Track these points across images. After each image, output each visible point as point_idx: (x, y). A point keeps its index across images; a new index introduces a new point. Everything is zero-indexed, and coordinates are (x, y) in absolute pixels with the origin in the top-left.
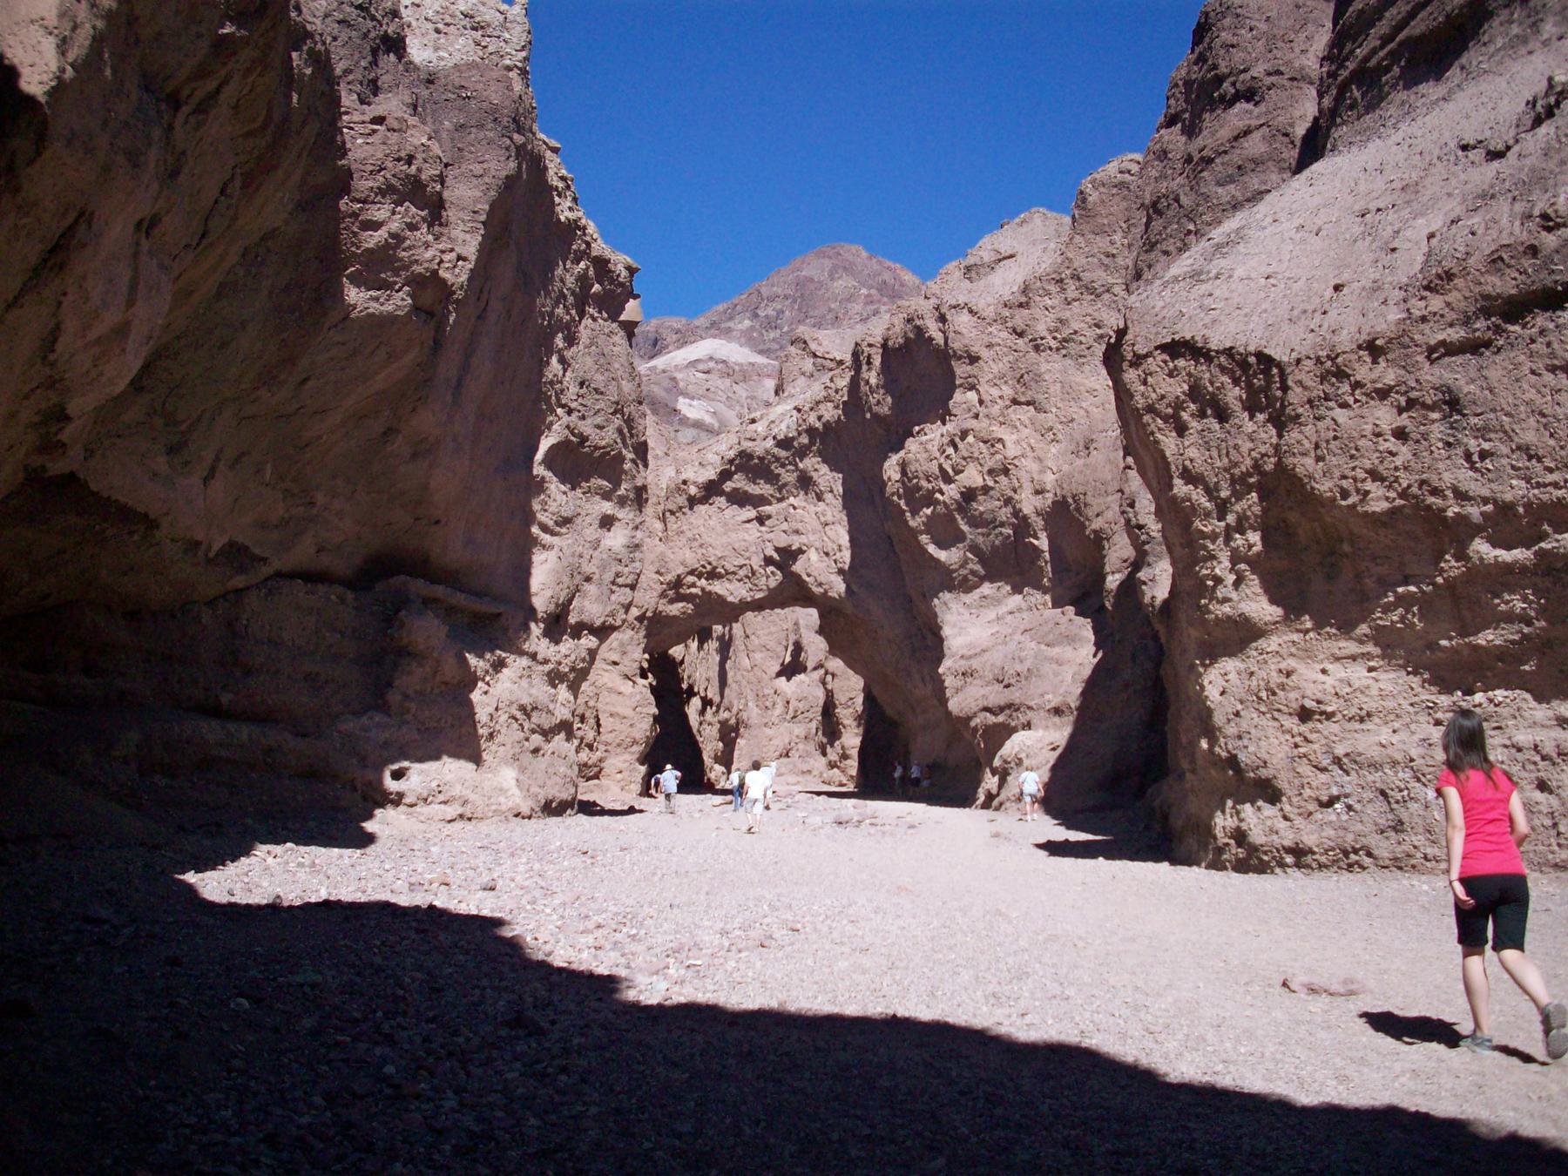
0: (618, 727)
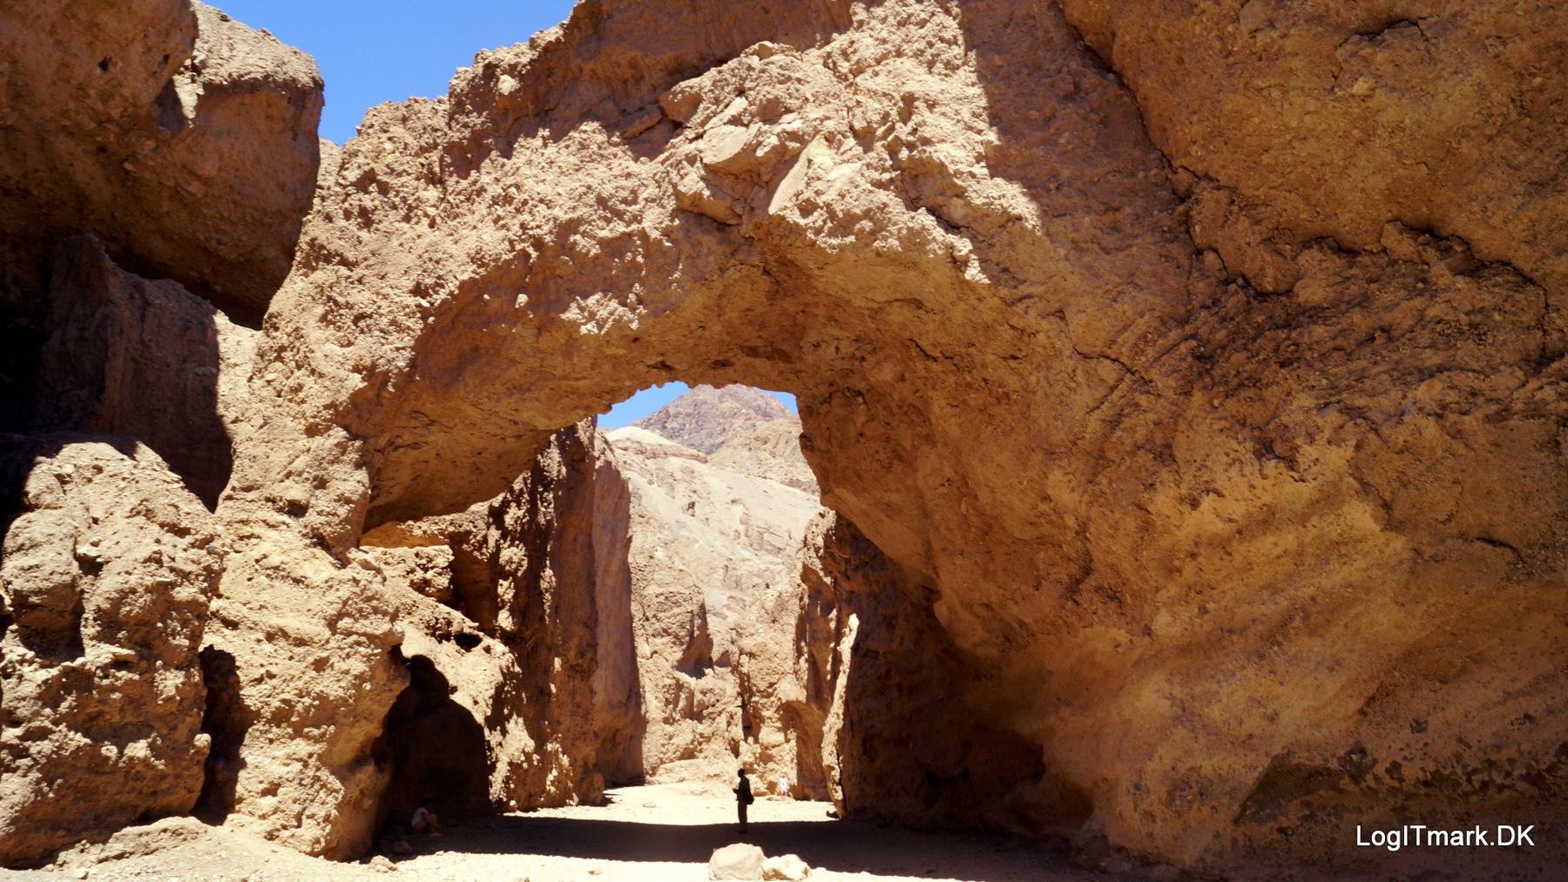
0: (281, 666)
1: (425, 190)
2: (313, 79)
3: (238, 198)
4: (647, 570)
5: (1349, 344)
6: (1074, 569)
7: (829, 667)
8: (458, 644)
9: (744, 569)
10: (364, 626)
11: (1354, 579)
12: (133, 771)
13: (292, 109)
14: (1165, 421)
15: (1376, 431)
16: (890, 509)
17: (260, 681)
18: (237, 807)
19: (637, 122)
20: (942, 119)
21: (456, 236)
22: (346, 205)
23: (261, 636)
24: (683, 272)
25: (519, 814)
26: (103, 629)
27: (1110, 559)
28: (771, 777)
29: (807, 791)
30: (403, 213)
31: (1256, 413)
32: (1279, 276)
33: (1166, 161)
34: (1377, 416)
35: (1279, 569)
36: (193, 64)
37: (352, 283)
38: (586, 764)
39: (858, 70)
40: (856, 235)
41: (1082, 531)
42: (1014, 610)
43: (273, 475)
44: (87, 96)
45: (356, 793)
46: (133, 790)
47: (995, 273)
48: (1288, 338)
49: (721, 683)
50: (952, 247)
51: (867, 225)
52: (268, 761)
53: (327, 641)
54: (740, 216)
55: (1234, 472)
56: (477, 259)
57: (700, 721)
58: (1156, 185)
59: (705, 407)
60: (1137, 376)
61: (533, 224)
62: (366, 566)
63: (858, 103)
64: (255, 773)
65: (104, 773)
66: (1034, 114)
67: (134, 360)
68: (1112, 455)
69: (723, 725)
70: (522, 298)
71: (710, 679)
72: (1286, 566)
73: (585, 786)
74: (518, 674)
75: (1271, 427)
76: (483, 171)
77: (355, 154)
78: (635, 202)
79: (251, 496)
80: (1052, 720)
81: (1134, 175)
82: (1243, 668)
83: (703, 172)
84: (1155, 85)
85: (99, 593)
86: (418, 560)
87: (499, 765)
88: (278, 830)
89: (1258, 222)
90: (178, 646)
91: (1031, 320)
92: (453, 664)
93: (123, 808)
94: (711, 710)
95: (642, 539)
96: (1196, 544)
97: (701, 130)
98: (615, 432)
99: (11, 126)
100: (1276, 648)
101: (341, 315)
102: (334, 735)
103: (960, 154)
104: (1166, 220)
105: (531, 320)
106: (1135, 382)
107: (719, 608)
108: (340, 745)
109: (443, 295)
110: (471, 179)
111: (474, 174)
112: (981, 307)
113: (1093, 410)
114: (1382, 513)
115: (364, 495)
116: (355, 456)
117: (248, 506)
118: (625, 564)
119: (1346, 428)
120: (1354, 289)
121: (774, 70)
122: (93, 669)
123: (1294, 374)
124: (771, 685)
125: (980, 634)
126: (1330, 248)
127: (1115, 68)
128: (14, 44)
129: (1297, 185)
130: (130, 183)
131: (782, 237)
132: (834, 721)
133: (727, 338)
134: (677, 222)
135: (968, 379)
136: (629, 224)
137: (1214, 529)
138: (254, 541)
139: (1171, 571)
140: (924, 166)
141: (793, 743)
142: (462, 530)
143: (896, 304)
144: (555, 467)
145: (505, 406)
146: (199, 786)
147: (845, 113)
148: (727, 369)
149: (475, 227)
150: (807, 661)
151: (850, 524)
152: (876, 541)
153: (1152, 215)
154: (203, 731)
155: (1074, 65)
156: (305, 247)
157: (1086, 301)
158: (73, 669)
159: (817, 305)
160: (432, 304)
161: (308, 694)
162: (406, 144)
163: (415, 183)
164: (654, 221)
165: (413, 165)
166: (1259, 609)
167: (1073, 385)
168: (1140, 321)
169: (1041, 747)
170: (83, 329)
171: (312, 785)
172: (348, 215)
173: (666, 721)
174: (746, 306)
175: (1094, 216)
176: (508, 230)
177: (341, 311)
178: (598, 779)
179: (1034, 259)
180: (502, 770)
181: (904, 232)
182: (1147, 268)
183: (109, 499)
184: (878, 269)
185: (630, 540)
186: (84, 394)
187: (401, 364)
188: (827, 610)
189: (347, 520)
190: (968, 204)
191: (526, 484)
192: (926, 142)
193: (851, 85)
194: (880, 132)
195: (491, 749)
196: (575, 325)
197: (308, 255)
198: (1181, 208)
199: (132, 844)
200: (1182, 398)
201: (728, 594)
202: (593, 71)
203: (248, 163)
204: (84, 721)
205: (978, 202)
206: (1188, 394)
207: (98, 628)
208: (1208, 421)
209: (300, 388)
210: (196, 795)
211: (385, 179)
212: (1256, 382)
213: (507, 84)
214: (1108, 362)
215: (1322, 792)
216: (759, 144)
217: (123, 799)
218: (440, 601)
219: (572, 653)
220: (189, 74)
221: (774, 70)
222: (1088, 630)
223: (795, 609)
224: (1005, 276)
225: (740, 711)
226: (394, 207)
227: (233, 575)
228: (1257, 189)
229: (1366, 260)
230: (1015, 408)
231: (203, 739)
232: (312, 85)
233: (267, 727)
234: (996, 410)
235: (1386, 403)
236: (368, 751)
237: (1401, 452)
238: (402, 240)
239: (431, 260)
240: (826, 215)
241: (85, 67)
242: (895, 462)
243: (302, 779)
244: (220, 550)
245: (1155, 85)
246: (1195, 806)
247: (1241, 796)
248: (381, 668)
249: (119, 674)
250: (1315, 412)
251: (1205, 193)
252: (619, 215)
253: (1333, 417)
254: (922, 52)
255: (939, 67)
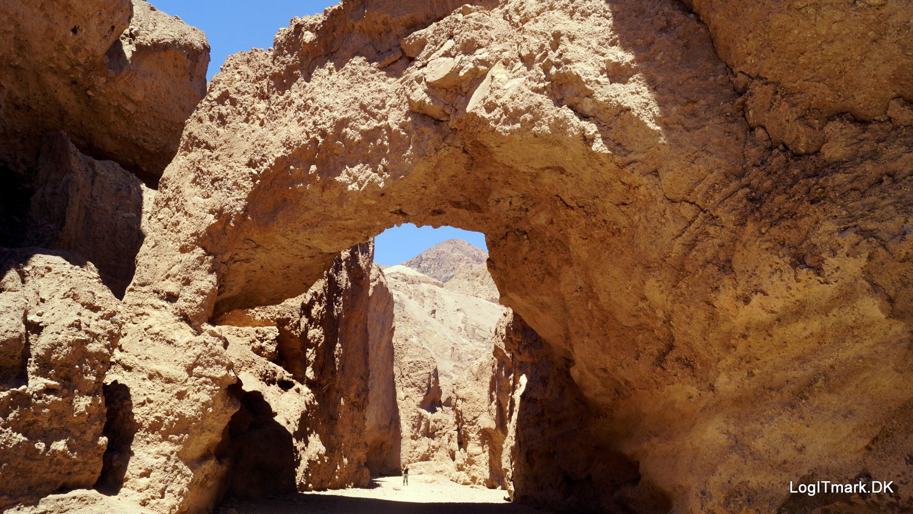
1: (258, 103)
2: (204, 45)
3: (156, 114)
4: (404, 347)
5: (863, 185)
6: (662, 346)
7: (508, 408)
8: (280, 386)
9: (463, 349)
10: (210, 372)
11: (864, 353)
12: (55, 459)
13: (189, 62)
14: (727, 244)
15: (884, 246)
16: (544, 307)
17: (143, 404)
18: (125, 484)
19: (387, 58)
20: (578, 47)
21: (275, 131)
22: (211, 112)
23: (145, 376)
24: (412, 151)
25: (314, 492)
26: (40, 368)
27: (686, 339)
28: (474, 474)
29: (494, 483)
30: (244, 117)
31: (793, 237)
32: (810, 142)
33: (729, 69)
34: (886, 236)
35: (806, 346)
36: (131, 33)
37: (212, 159)
38: (359, 462)
39: (525, 20)
40: (521, 123)
41: (668, 321)
42: (622, 372)
43: (159, 277)
44: (64, 49)
45: (201, 477)
46: (55, 471)
47: (612, 146)
48: (817, 183)
49: (446, 416)
50: (584, 130)
51: (528, 116)
52: (145, 455)
53: (186, 381)
54: (449, 115)
55: (775, 278)
56: (287, 144)
57: (433, 438)
58: (722, 85)
59: (443, 255)
60: (708, 213)
61: (321, 122)
62: (213, 334)
63: (524, 39)
64: (136, 463)
65: (36, 460)
66: (640, 41)
67: (86, 207)
68: (689, 268)
69: (446, 441)
70: (313, 168)
71: (439, 414)
72: (813, 343)
73: (358, 475)
74: (316, 406)
75: (803, 246)
76: (293, 90)
77: (218, 82)
78: (383, 107)
79: (144, 289)
80: (646, 445)
81: (707, 79)
82: (780, 414)
83: (426, 88)
84: (723, 17)
85: (39, 345)
86: (257, 335)
87: (302, 462)
88: (149, 499)
89: (795, 105)
90: (88, 380)
91: (636, 178)
92: (275, 399)
93: (48, 483)
94: (439, 432)
95: (401, 331)
96: (747, 329)
97: (425, 62)
98: (388, 269)
99: (18, 66)
100: (804, 401)
101: (204, 179)
102: (188, 440)
103: (590, 69)
104: (728, 108)
105: (318, 182)
106: (706, 218)
107: (448, 372)
108: (191, 447)
109: (265, 166)
110: (285, 95)
111: (287, 92)
112: (603, 170)
113: (677, 237)
114: (887, 305)
115: (213, 290)
116: (209, 266)
117: (142, 295)
118: (390, 342)
119: (861, 244)
120: (867, 147)
121: (472, 21)
122: (31, 393)
123: (821, 209)
124: (475, 418)
125: (599, 388)
126: (848, 119)
127: (694, 10)
128: (17, 14)
129: (824, 77)
130: (91, 104)
131: (474, 127)
132: (509, 442)
133: (441, 195)
134: (409, 119)
135: (594, 220)
136: (379, 121)
137: (761, 319)
138: (145, 317)
139: (729, 347)
140: (566, 78)
141: (487, 453)
142: (284, 317)
143: (547, 171)
144: (345, 282)
145: (302, 237)
146: (99, 470)
147: (516, 47)
148: (441, 216)
149: (286, 125)
150: (496, 404)
151: (521, 320)
152: (534, 328)
153: (719, 105)
154: (103, 435)
155: (666, 10)
156: (186, 138)
157: (673, 163)
158: (18, 393)
159: (497, 173)
160: (259, 172)
161: (172, 413)
162: (248, 75)
163: (252, 99)
164: (395, 118)
165: (252, 88)
166: (791, 374)
167: (663, 221)
168: (710, 176)
169: (638, 463)
170: (55, 188)
171: (172, 472)
172: (211, 118)
173: (413, 438)
174: (452, 173)
175: (679, 107)
176: (306, 126)
177: (205, 177)
178: (366, 472)
179: (638, 136)
180: (304, 464)
181: (552, 120)
182: (716, 140)
183: (53, 288)
184: (536, 146)
185: (394, 329)
186: (52, 226)
187: (239, 209)
188: (508, 373)
189: (201, 305)
190: (595, 101)
191: (325, 291)
192: (568, 62)
193: (520, 30)
194: (538, 57)
195: (297, 452)
196: (344, 185)
197: (187, 143)
198: (740, 100)
199: (52, 506)
200: (739, 228)
201: (454, 364)
202: (361, 27)
203: (162, 94)
204: (24, 426)
205: (601, 100)
206: (743, 225)
207: (37, 367)
208: (758, 243)
209: (178, 223)
210: (97, 476)
211: (234, 96)
212: (792, 215)
213: (308, 36)
214: (687, 205)
215: (837, 503)
216: (461, 68)
217: (48, 476)
218: (270, 360)
219: (352, 395)
220: (128, 39)
221: (472, 21)
222: (671, 387)
223: (489, 373)
224: (619, 148)
225: (456, 433)
226: (240, 113)
227: (131, 338)
228: (795, 82)
229: (876, 126)
230: (624, 238)
231: (103, 440)
232: (202, 48)
233: (146, 433)
234: (611, 240)
235: (892, 226)
236: (212, 451)
237: (903, 261)
238: (243, 133)
239: (259, 145)
240: (502, 111)
241: (63, 31)
242: (547, 276)
243: (166, 468)
244: (119, 321)
245: (723, 17)
246: (744, 508)
247: (778, 503)
248: (219, 399)
249: (49, 397)
250: (837, 234)
251: (757, 88)
252: (374, 115)
253: (852, 236)
254: (567, 6)
255: (578, 14)
